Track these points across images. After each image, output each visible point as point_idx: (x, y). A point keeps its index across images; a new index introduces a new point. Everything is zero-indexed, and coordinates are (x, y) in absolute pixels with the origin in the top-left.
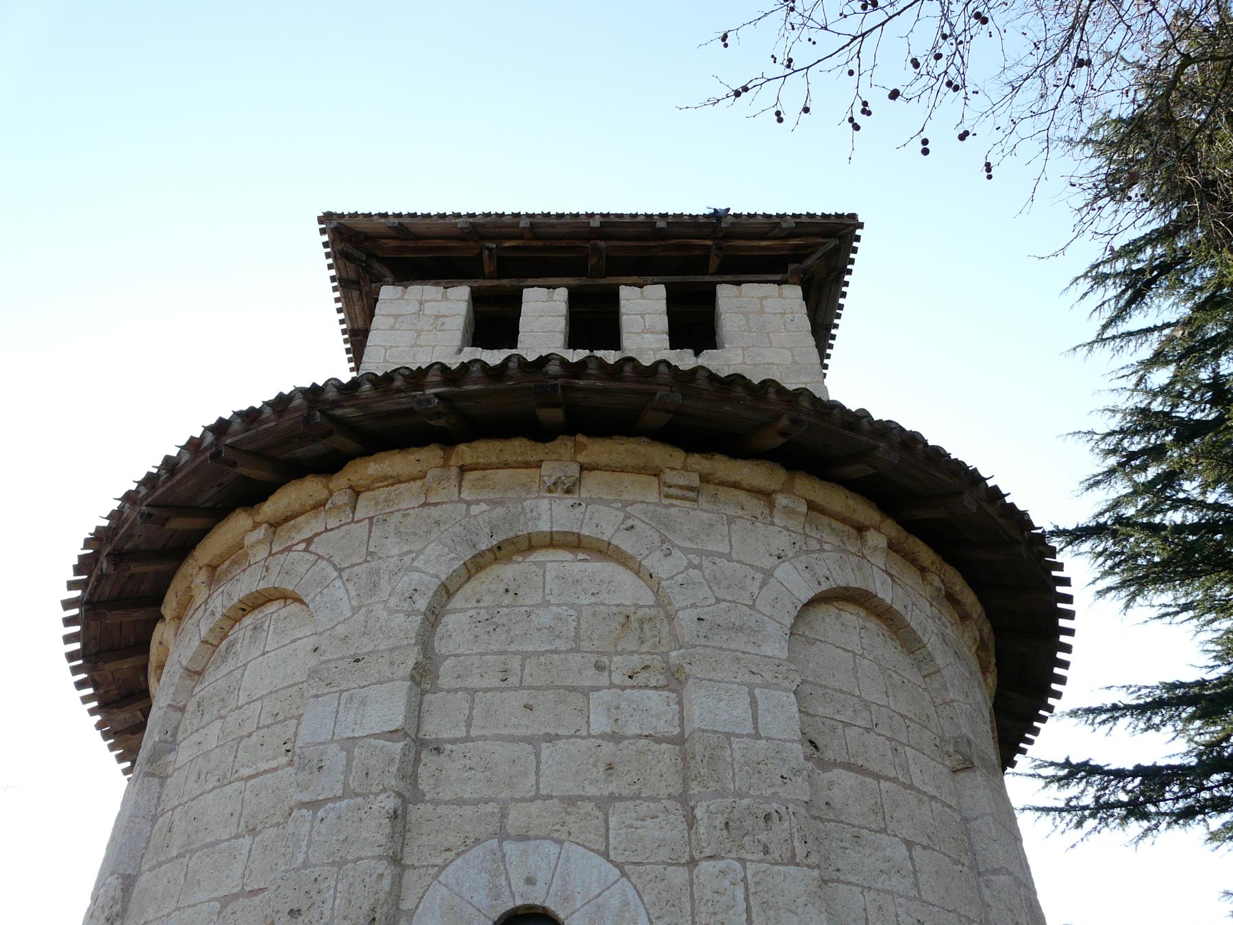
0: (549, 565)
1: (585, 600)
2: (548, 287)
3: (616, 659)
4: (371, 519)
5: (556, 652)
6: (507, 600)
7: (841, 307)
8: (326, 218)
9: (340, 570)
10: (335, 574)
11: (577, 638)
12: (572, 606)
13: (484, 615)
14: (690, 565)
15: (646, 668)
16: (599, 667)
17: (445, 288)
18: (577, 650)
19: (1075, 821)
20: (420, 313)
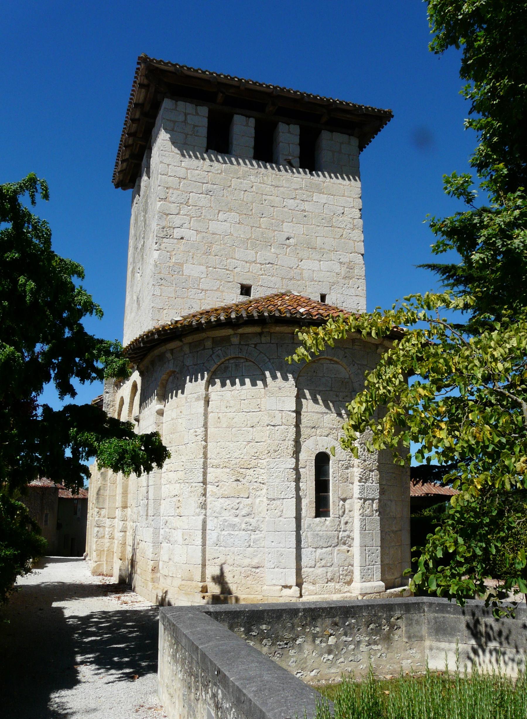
0: (324, 365)
1: (333, 376)
2: (246, 116)
3: (341, 393)
4: (277, 344)
5: (327, 391)
6: (315, 374)
7: (371, 142)
8: (144, 60)
9: (269, 359)
10: (268, 360)
11: (331, 387)
12: (330, 377)
13: (309, 378)
14: (359, 369)
15: (347, 396)
16: (337, 396)
17: (196, 105)
18: (331, 390)
19: (491, 633)
20: (185, 121)
